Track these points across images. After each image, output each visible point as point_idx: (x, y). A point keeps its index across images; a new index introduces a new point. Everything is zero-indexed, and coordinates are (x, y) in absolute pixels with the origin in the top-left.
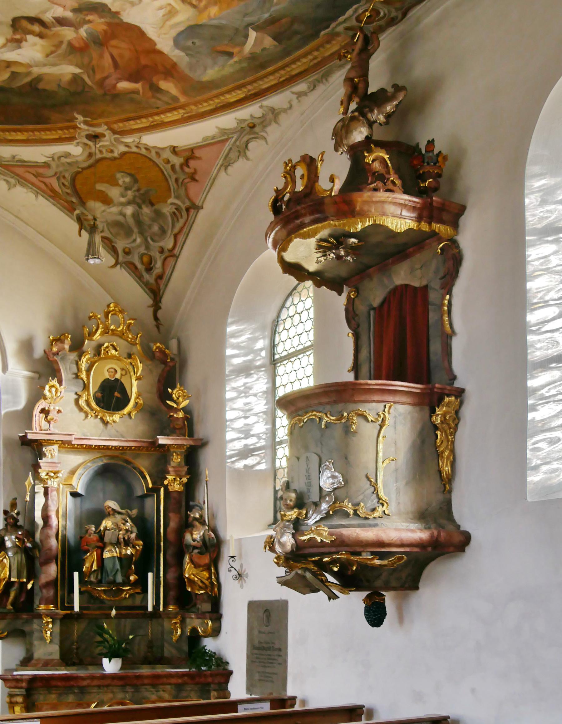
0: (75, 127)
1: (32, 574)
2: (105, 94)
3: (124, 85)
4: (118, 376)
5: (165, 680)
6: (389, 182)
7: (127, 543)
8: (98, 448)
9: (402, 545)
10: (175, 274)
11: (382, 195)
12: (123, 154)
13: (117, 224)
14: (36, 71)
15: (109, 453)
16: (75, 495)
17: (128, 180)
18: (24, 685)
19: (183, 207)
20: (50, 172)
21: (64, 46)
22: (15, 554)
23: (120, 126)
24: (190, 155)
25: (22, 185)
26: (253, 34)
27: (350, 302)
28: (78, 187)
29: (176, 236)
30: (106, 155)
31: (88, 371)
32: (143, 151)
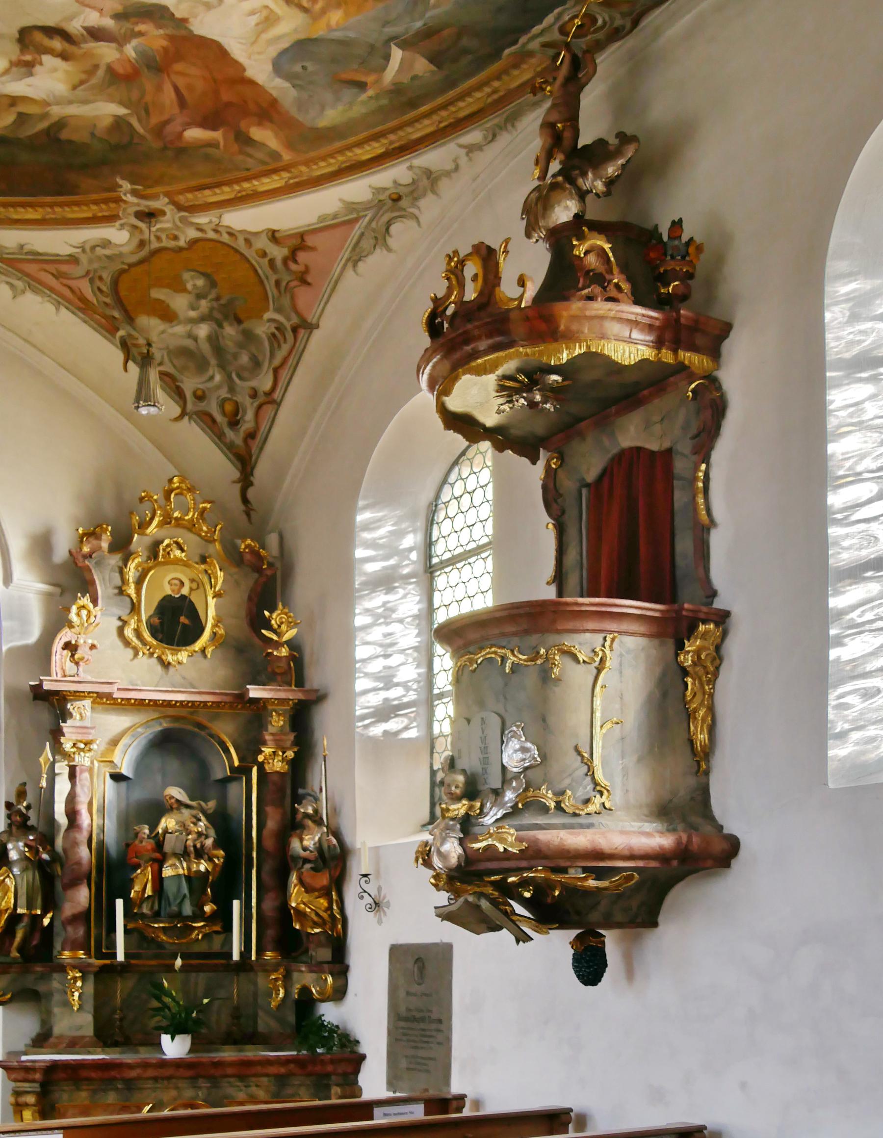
0: (118, 200)
1: (50, 902)
2: (165, 148)
3: (194, 134)
4: (185, 591)
5: (259, 1069)
6: (611, 287)
7: (200, 853)
8: (155, 704)
9: (632, 857)
10: (275, 431)
11: (600, 307)
12: (194, 242)
13: (184, 352)
14: (57, 111)
15: (171, 712)
16: (117, 777)
17: (200, 282)
18: (38, 1076)
19: (288, 325)
20: (79, 271)
21: (101, 73)
22: (24, 870)
23: (188, 198)
24: (298, 243)
25: (35, 291)
26: (397, 54)
27: (550, 475)
28: (123, 293)
29: (276, 371)
30: (166, 243)
31: (139, 583)
32: (225, 238)
